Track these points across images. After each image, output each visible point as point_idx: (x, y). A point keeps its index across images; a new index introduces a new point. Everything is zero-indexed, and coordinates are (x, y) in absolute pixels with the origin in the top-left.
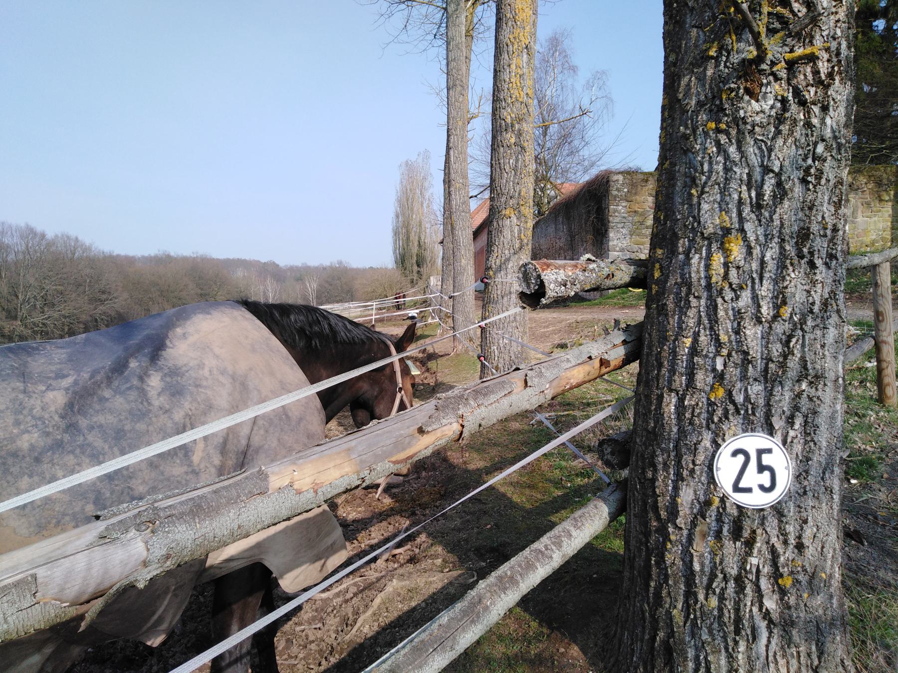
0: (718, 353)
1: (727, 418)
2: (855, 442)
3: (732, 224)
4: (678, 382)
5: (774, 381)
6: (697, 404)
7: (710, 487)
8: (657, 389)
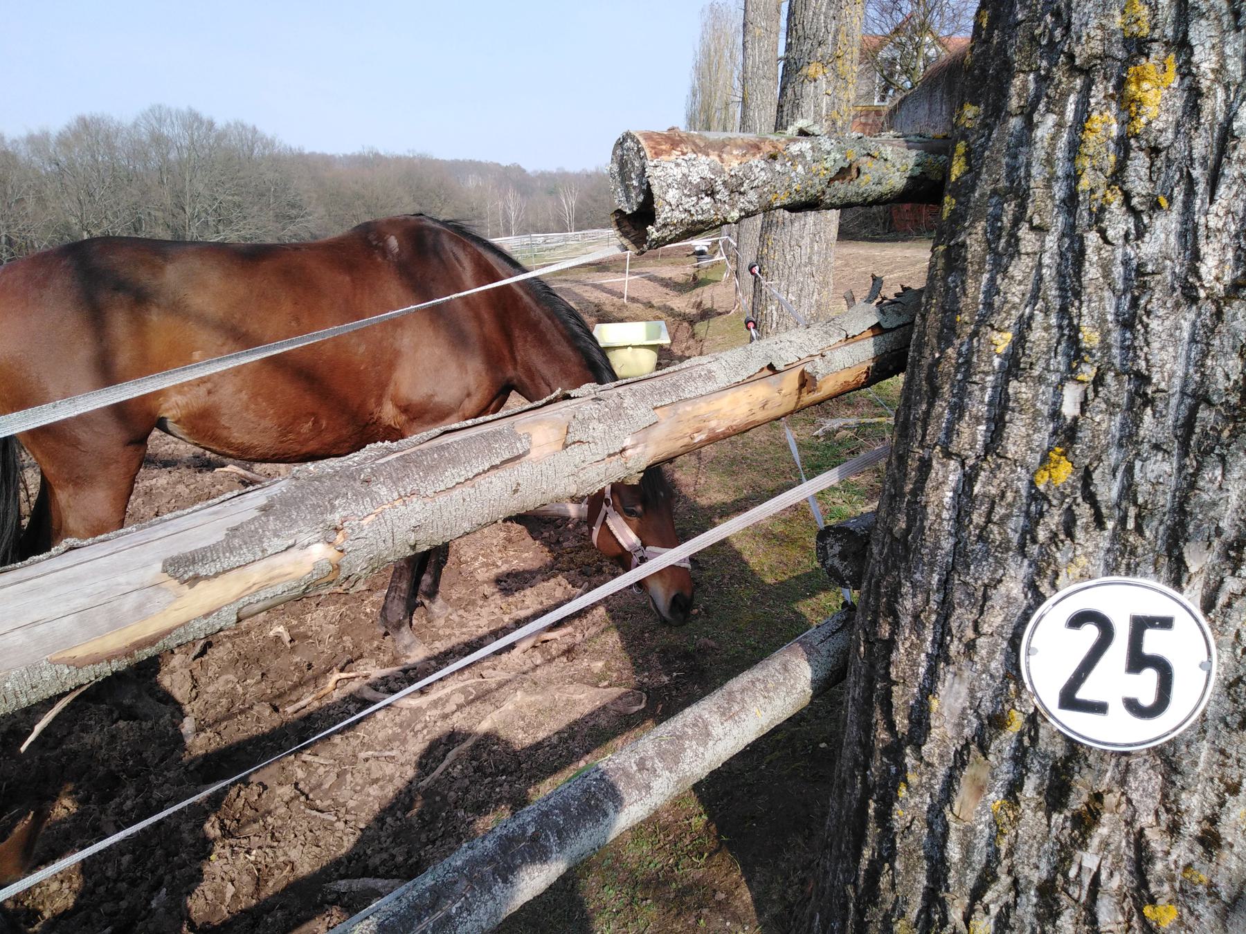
0: (1071, 373)
1: (1070, 535)
3: (1153, 28)
5: (1208, 452)
6: (1003, 495)
7: (1007, 688)
8: (922, 447)
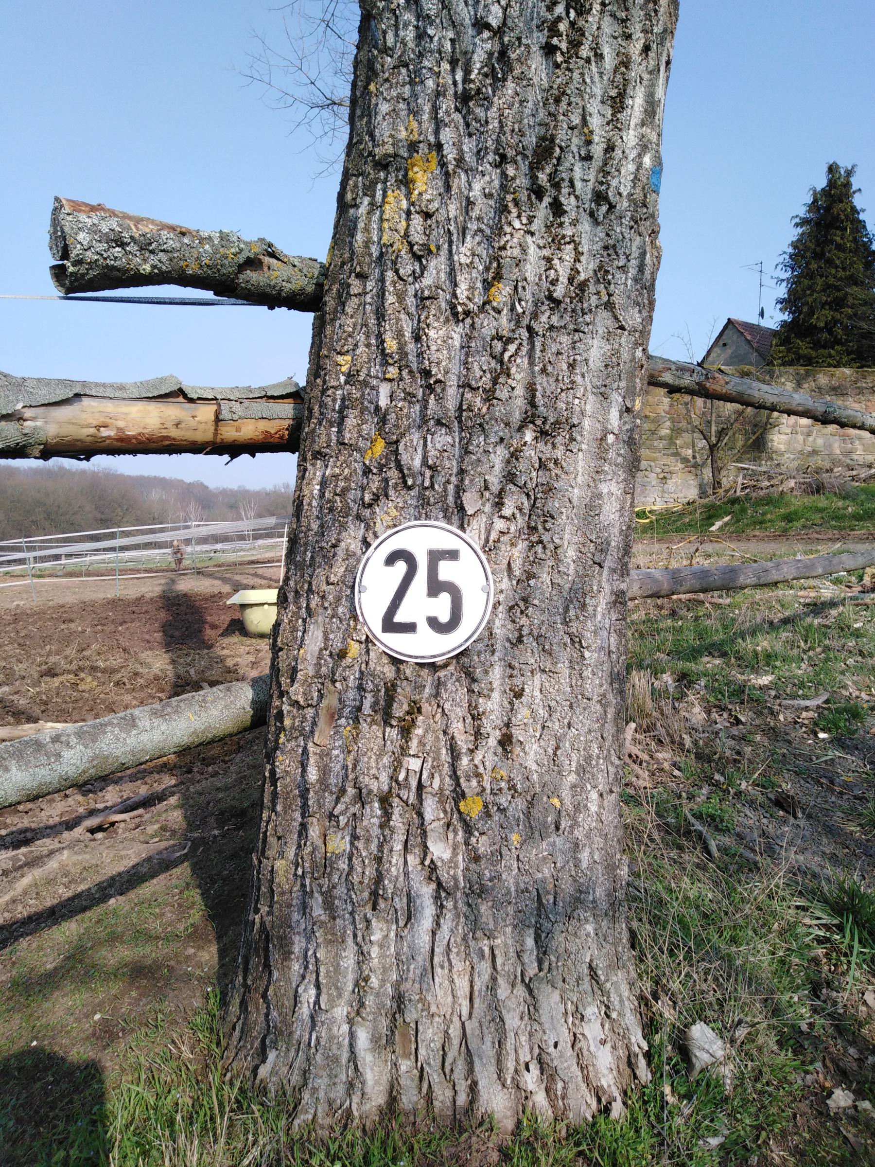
2: (845, 687)
3: (420, 135)
4: (324, 438)
